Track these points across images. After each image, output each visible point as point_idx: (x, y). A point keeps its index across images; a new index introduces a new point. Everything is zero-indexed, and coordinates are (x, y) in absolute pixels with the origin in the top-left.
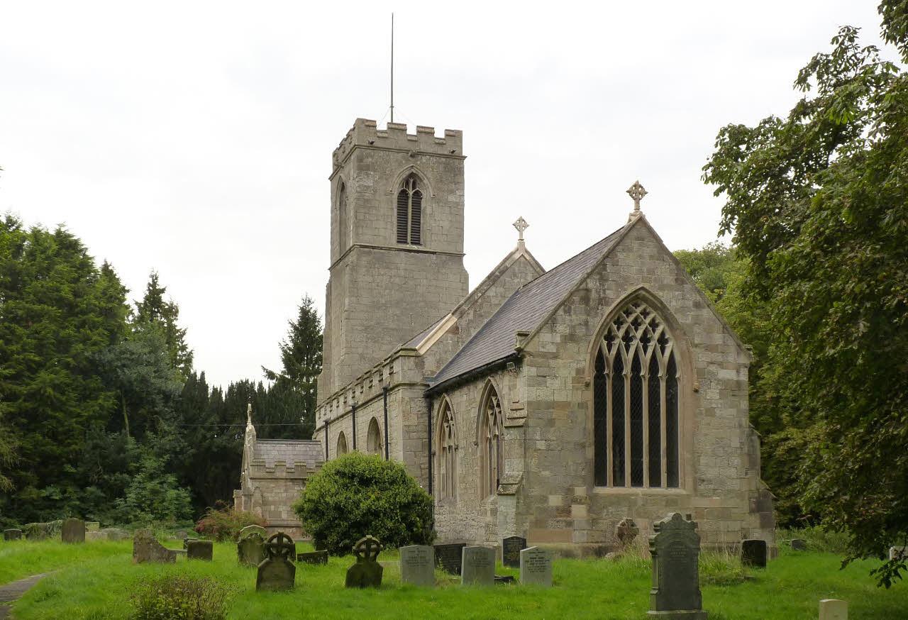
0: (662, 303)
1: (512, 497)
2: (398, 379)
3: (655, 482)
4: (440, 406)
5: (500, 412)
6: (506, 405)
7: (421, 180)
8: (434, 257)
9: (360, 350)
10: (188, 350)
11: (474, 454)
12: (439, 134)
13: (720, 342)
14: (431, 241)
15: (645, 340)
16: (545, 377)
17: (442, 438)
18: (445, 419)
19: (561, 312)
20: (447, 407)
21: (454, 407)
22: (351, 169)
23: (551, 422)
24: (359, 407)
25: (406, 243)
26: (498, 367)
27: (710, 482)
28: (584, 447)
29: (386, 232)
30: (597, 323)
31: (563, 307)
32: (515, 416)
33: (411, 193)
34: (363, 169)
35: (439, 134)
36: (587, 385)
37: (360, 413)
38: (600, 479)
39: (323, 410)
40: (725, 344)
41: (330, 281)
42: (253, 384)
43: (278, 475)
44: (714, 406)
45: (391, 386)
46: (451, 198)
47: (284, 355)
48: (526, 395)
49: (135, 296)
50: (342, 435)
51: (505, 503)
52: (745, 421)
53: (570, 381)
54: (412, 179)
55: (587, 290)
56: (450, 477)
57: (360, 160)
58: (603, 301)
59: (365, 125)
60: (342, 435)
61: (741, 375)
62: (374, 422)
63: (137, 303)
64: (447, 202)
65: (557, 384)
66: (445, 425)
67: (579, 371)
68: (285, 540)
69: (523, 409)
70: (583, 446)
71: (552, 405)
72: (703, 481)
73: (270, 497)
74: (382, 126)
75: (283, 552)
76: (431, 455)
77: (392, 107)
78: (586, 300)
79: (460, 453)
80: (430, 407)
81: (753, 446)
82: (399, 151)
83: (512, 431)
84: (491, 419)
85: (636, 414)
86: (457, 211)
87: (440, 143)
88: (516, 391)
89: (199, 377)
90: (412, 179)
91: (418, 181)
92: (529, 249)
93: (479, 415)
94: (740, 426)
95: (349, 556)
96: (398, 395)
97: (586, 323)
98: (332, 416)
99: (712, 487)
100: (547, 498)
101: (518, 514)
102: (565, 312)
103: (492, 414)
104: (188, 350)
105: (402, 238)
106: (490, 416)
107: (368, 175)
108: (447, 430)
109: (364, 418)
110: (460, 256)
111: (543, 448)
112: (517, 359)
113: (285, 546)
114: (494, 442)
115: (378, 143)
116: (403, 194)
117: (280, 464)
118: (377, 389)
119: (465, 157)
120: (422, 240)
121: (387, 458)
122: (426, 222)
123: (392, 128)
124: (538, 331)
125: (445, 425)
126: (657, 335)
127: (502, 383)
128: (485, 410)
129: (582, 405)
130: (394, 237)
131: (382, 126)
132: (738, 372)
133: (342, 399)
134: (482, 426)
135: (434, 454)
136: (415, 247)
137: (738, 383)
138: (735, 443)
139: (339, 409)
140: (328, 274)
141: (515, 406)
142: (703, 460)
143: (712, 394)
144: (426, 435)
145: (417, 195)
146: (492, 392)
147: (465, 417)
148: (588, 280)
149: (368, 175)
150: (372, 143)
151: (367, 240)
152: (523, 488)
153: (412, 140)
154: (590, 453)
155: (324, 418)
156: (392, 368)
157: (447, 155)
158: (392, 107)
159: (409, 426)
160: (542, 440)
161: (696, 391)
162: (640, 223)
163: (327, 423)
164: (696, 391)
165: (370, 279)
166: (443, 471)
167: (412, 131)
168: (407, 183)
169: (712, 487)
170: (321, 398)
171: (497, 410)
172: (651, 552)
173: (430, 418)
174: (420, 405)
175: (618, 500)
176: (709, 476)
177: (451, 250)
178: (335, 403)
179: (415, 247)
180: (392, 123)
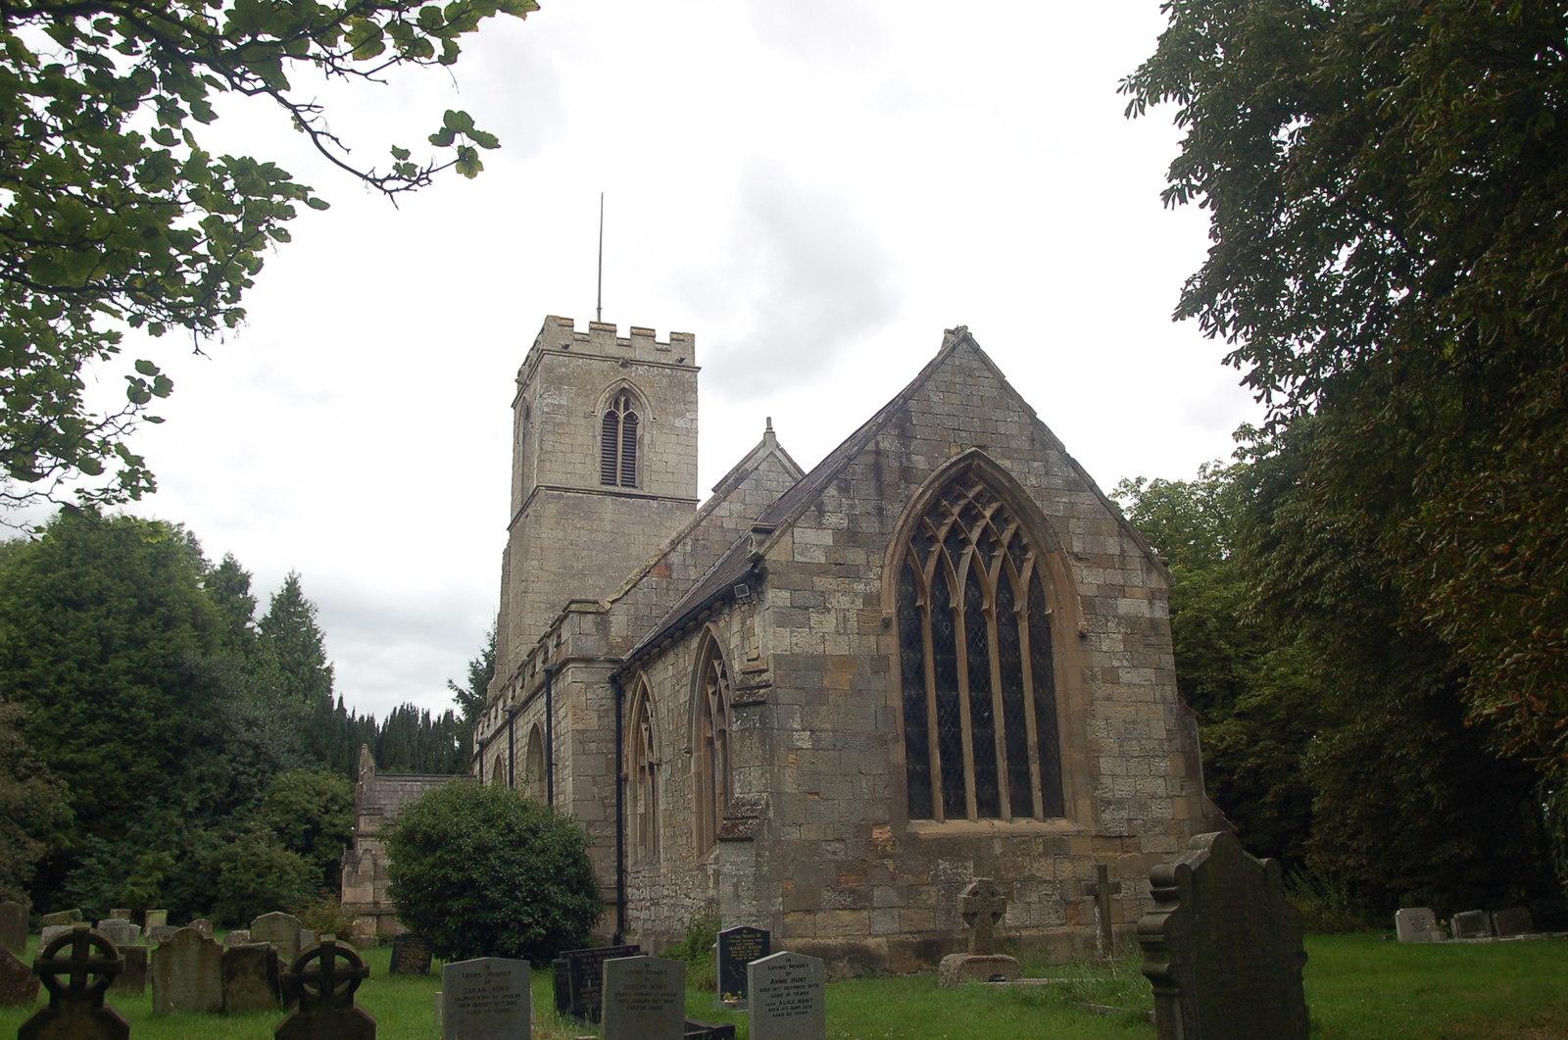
0: (1011, 480)
1: (747, 845)
2: (569, 650)
3: (1022, 808)
5: (727, 687)
8: (654, 504)
10: (327, 664)
11: (686, 768)
12: (663, 337)
14: (651, 481)
15: (987, 543)
16: (807, 608)
17: (639, 751)
18: (643, 716)
19: (832, 491)
20: (645, 695)
21: (654, 692)
22: (537, 384)
23: (820, 696)
25: (615, 484)
26: (722, 601)
27: (1120, 803)
28: (886, 743)
29: (579, 460)
30: (899, 516)
31: (835, 482)
32: (753, 683)
33: (622, 415)
35: (663, 337)
36: (886, 624)
40: (1123, 554)
41: (509, 546)
44: (1116, 663)
47: (473, 674)
49: (263, 592)
52: (1171, 691)
53: (852, 616)
54: (624, 396)
55: (878, 453)
58: (907, 474)
59: (557, 326)
61: (1156, 607)
64: (673, 427)
65: (830, 622)
66: (644, 726)
67: (872, 600)
68: (92, 950)
69: (766, 671)
70: (883, 741)
71: (818, 663)
72: (1109, 803)
74: (581, 327)
76: (621, 781)
77: (599, 309)
78: (877, 470)
79: (662, 776)
80: (619, 696)
81: (1189, 736)
82: (605, 358)
87: (663, 349)
88: (756, 638)
90: (624, 396)
92: (783, 445)
93: (692, 697)
94: (1164, 701)
96: (571, 676)
97: (880, 510)
98: (488, 734)
99: (1124, 814)
101: (759, 878)
102: (840, 489)
103: (714, 693)
105: (608, 478)
107: (559, 389)
108: (646, 734)
109: (523, 728)
111: (808, 745)
112: (756, 577)
115: (575, 348)
116: (611, 417)
119: (699, 368)
120: (637, 481)
122: (646, 455)
123: (595, 329)
125: (644, 726)
127: (729, 630)
129: (879, 663)
131: (581, 327)
132: (1150, 602)
134: (698, 718)
135: (626, 780)
136: (627, 490)
137: (1154, 624)
138: (1159, 730)
140: (507, 535)
143: (1111, 642)
144: (612, 746)
145: (631, 418)
146: (713, 651)
149: (559, 389)
150: (567, 347)
151: (556, 478)
152: (769, 825)
153: (622, 343)
156: (559, 636)
157: (674, 364)
158: (599, 309)
159: (583, 732)
160: (804, 730)
161: (1083, 636)
164: (1083, 636)
165: (560, 534)
166: (641, 810)
167: (623, 332)
169: (1124, 814)
171: (722, 683)
172: (1154, 977)
173: (619, 717)
174: (603, 693)
175: (952, 848)
176: (1118, 794)
177: (681, 493)
179: (627, 490)
180: (599, 323)
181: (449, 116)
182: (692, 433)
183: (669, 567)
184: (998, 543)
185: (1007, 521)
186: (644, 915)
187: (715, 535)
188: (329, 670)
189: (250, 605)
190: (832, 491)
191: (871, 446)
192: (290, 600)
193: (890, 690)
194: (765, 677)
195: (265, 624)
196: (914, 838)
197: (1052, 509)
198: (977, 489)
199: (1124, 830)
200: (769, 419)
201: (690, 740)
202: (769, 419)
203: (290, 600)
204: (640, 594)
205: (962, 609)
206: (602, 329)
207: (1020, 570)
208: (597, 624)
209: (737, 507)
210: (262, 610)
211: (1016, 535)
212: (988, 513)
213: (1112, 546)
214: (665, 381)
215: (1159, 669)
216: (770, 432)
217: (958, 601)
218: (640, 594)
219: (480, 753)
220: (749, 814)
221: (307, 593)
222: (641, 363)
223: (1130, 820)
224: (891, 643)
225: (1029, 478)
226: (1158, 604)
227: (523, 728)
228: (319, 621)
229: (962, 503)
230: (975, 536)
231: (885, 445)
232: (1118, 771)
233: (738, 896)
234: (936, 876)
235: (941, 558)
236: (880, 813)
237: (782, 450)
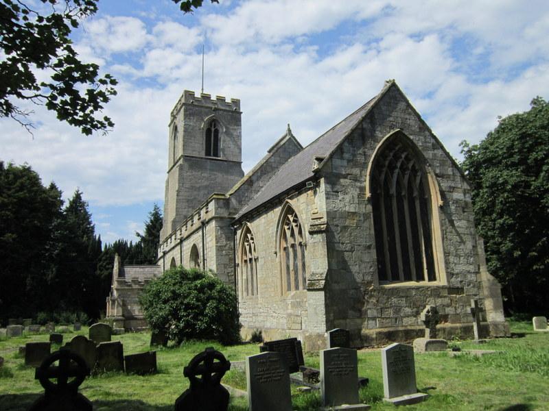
4: (242, 231)
7: (219, 123)
9: (184, 213)
10: (92, 225)
13: (451, 173)
24: (185, 239)
25: (210, 155)
29: (199, 150)
32: (317, 223)
33: (213, 129)
34: (187, 116)
37: (185, 243)
39: (162, 246)
42: (126, 243)
45: (207, 220)
48: (324, 207)
49: (67, 197)
50: (173, 260)
51: (314, 297)
57: (185, 111)
60: (173, 260)
62: (194, 248)
63: (69, 199)
66: (246, 244)
69: (322, 218)
70: (369, 247)
75: (51, 380)
84: (288, 233)
86: (237, 140)
87: (228, 105)
89: (97, 238)
91: (217, 124)
95: (187, 365)
98: (167, 249)
100: (51, 340)
103: (289, 229)
104: (92, 225)
105: (208, 153)
106: (286, 230)
109: (188, 246)
110: (240, 163)
114: (298, 249)
116: (208, 131)
118: (197, 224)
121: (204, 269)
122: (221, 145)
125: (246, 244)
126: (410, 165)
127: (299, 204)
128: (282, 226)
129: (366, 216)
132: (465, 195)
133: (173, 237)
136: (214, 158)
139: (173, 242)
145: (217, 132)
146: (290, 210)
147: (264, 235)
148: (363, 123)
154: (374, 252)
155: (162, 251)
162: (393, 88)
163: (165, 253)
166: (244, 277)
168: (211, 126)
170: (162, 239)
178: (169, 240)
179: (214, 158)
181: (49, 109)
184: (407, 168)
185: (410, 160)
186: (248, 319)
188: (93, 228)
189: (62, 203)
190: (346, 144)
191: (360, 126)
192: (77, 202)
193: (368, 228)
194: (322, 220)
195: (68, 210)
196: (383, 289)
197: (429, 154)
198: (399, 146)
199: (459, 285)
200: (289, 125)
201: (276, 248)
202: (289, 125)
203: (77, 202)
204: (241, 193)
205: (395, 194)
206: (206, 97)
207: (415, 179)
208: (224, 203)
210: (66, 205)
211: (413, 166)
212: (403, 156)
213: (450, 171)
214: (229, 117)
215: (468, 221)
216: (289, 130)
217: (393, 191)
218: (241, 193)
219: (163, 257)
220: (319, 278)
221: (84, 198)
223: (461, 282)
224: (370, 208)
225: (419, 141)
226: (467, 195)
227: (188, 246)
228: (90, 210)
229: (394, 151)
230: (399, 165)
231: (365, 126)
232: (455, 261)
233: (316, 313)
234: (391, 304)
235: (386, 173)
236: (368, 278)
237: (294, 137)
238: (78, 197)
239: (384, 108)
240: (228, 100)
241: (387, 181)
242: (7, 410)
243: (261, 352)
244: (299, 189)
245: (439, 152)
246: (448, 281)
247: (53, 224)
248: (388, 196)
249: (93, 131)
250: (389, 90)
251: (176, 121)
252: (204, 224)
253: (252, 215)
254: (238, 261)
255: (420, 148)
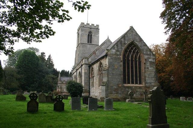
6: (104, 65)
11: (97, 77)
15: (134, 52)
17: (92, 75)
21: (94, 68)
26: (103, 58)
27: (148, 83)
29: (85, 40)
30: (124, 48)
34: (82, 30)
35: (95, 25)
36: (121, 61)
38: (125, 82)
43: (64, 83)
46: (97, 36)
54: (90, 32)
56: (93, 82)
57: (81, 29)
58: (125, 44)
59: (83, 23)
70: (121, 75)
73: (62, 87)
76: (90, 78)
80: (90, 68)
82: (88, 28)
83: (105, 71)
85: (128, 72)
87: (95, 27)
90: (90, 32)
96: (84, 66)
105: (88, 42)
113: (35, 97)
116: (89, 35)
117: (64, 81)
124: (111, 49)
127: (103, 61)
130: (87, 42)
140: (76, 49)
141: (106, 66)
142: (147, 78)
145: (91, 35)
146: (101, 64)
151: (82, 42)
153: (91, 26)
154: (122, 76)
161: (145, 63)
166: (92, 81)
171: (102, 67)
173: (90, 71)
174: (87, 68)
177: (97, 44)
182: (98, 37)
183: (96, 53)
187: (101, 50)
196: (124, 86)
206: (88, 24)
209: (104, 46)
211: (137, 51)
213: (149, 53)
216: (108, 38)
217: (130, 59)
219: (73, 74)
222: (93, 28)
225: (139, 44)
226: (154, 60)
230: (132, 51)
235: (128, 54)
236: (120, 83)
238: (50, 56)
239: (128, 34)
240: (95, 25)
241: (128, 56)
242: (48, 127)
243: (104, 102)
244: (103, 58)
245: (145, 47)
246: (145, 85)
247: (20, 76)
248: (128, 60)
249: (70, 19)
250: (130, 29)
251: (79, 32)
252: (82, 65)
253: (93, 64)
254: (91, 77)
255: (139, 46)
